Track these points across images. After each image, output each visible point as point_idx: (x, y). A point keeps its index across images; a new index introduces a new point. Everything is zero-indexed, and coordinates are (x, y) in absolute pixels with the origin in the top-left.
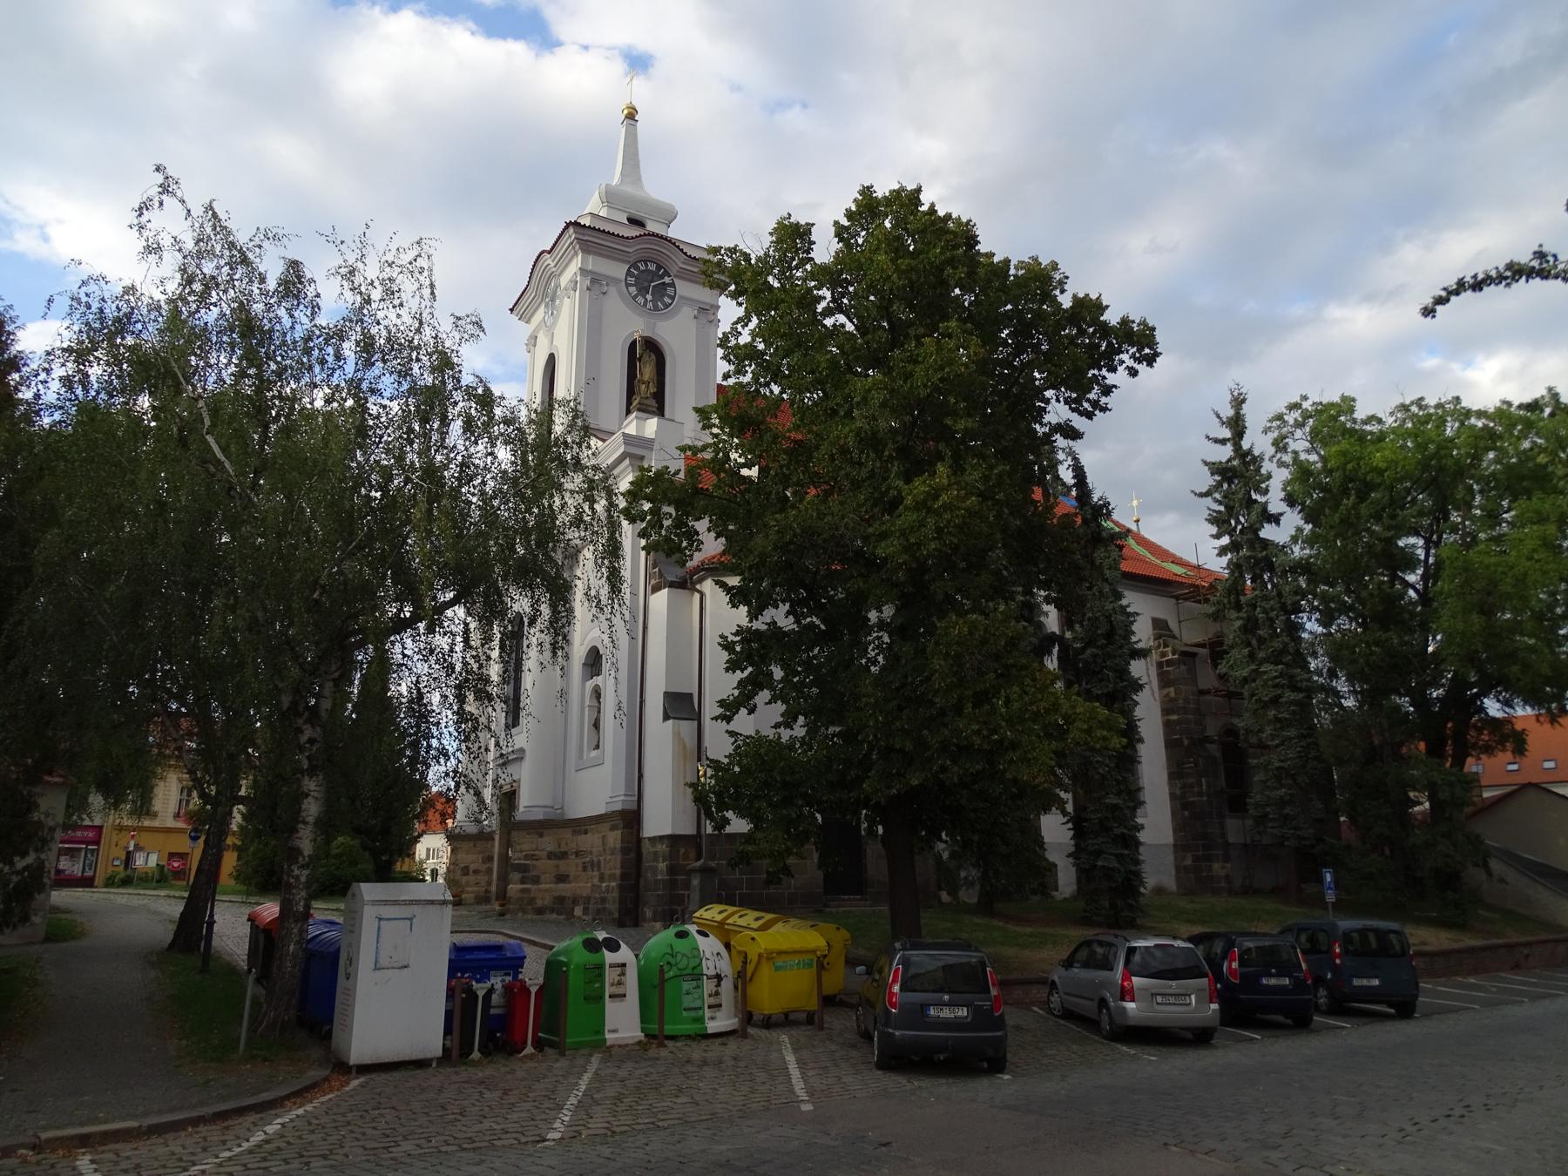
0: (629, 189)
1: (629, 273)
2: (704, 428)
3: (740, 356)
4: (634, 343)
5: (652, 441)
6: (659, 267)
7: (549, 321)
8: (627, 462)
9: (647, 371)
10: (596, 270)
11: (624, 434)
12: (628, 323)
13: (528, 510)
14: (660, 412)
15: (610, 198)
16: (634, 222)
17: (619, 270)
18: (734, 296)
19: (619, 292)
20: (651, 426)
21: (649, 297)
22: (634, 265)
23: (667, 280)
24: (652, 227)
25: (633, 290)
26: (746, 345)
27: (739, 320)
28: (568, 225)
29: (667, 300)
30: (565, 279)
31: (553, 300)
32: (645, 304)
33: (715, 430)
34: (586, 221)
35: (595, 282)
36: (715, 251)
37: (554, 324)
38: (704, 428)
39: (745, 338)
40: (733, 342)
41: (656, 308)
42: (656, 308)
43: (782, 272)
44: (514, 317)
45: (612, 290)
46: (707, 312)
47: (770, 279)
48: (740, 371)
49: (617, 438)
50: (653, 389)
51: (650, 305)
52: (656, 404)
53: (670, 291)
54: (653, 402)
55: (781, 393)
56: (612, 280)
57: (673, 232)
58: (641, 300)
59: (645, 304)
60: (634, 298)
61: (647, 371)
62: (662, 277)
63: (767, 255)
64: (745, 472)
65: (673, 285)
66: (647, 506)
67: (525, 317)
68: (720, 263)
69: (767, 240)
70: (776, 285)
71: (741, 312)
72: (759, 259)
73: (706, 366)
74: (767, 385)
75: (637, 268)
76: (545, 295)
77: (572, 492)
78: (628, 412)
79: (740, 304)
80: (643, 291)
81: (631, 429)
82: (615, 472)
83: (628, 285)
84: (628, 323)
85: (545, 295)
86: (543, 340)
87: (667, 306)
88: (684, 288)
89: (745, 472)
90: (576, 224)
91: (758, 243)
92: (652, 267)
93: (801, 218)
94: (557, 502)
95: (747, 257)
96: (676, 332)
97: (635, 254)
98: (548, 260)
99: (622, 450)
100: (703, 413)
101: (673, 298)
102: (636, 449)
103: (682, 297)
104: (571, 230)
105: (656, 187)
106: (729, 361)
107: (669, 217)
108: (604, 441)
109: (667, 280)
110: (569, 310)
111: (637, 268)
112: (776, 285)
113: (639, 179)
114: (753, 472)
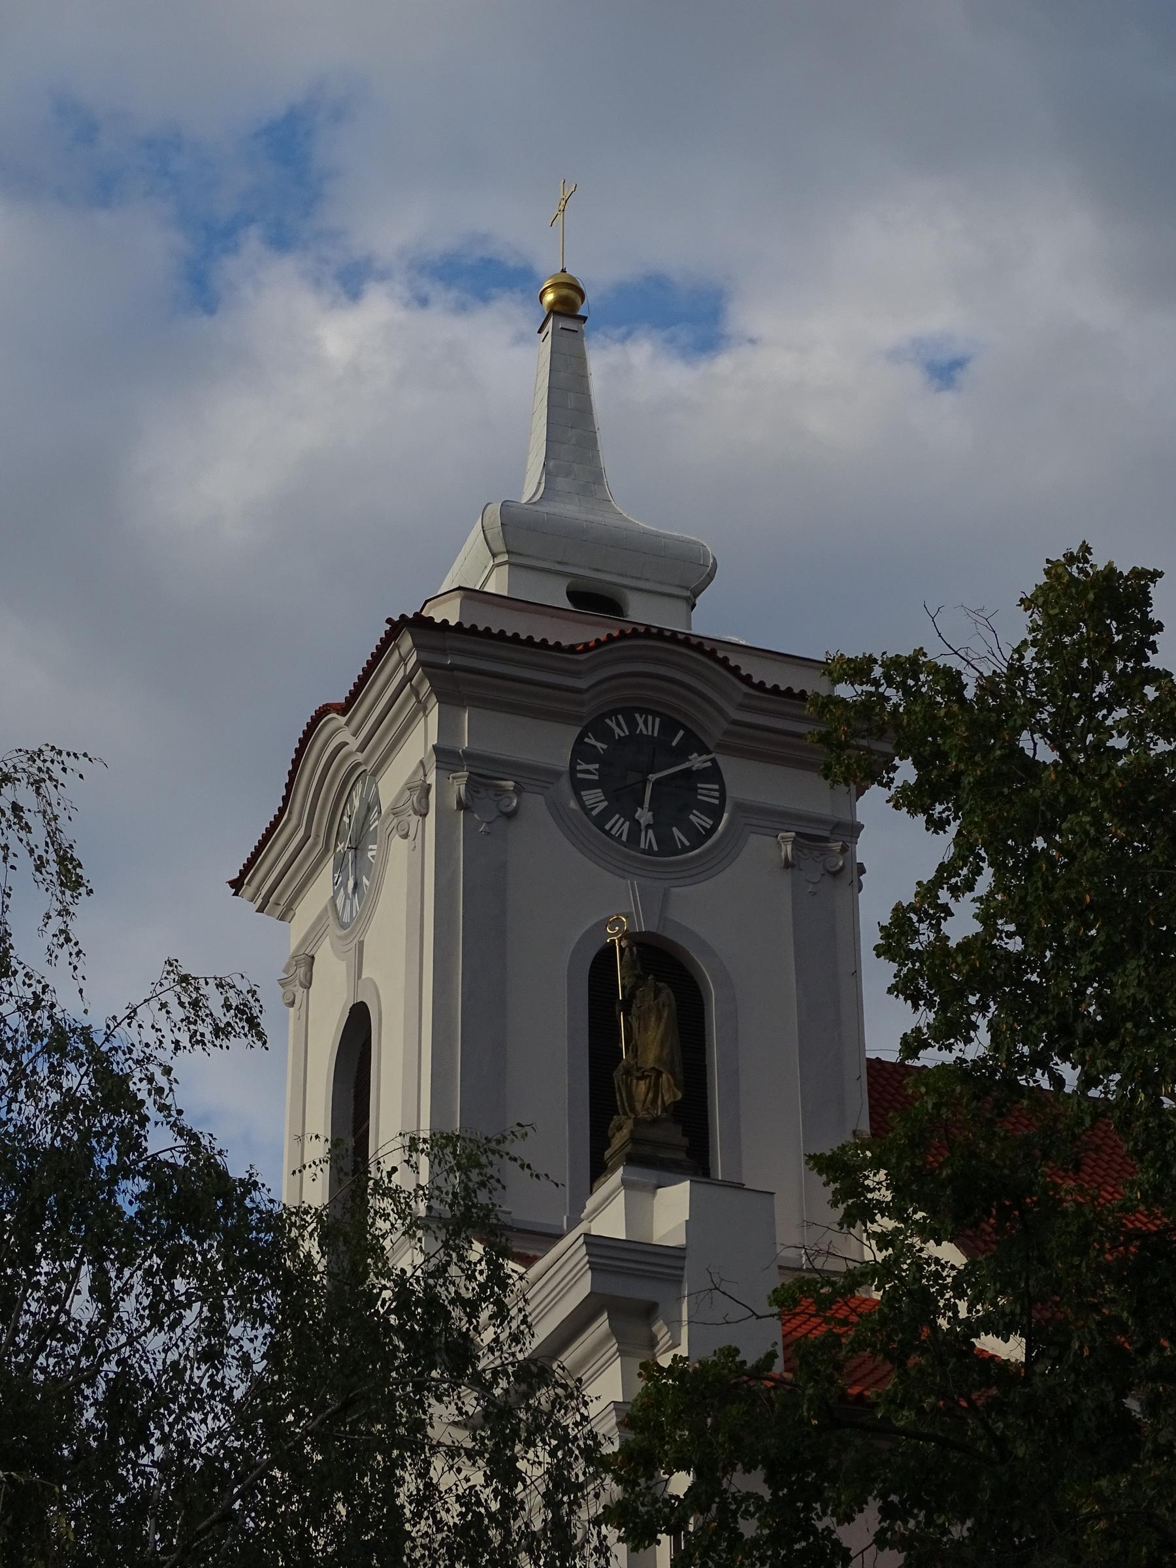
0: (570, 510)
1: (580, 751)
2: (848, 1220)
3: (940, 979)
4: (604, 959)
5: (676, 1255)
6: (670, 726)
7: (349, 908)
8: (602, 1325)
9: (648, 1041)
10: (489, 748)
11: (593, 1242)
12: (589, 899)
13: (317, 1510)
14: (694, 1160)
15: (518, 536)
16: (592, 600)
17: (550, 745)
18: (912, 800)
19: (557, 810)
20: (671, 1211)
21: (644, 816)
22: (596, 727)
23: (697, 761)
24: (642, 611)
25: (595, 798)
26: (966, 946)
27: (945, 871)
28: (396, 628)
29: (698, 819)
30: (392, 784)
31: (357, 847)
32: (634, 837)
33: (886, 1224)
34: (448, 612)
35: (481, 787)
36: (858, 670)
37: (364, 917)
38: (848, 1220)
39: (962, 924)
40: (926, 935)
41: (667, 846)
42: (667, 846)
43: (1064, 719)
44: (245, 906)
45: (535, 803)
46: (826, 852)
47: (1025, 741)
48: (952, 1028)
49: (569, 1253)
50: (670, 1094)
51: (648, 838)
52: (679, 1142)
53: (707, 792)
54: (675, 1134)
55: (1088, 1081)
56: (532, 777)
57: (708, 620)
58: (619, 826)
59: (634, 837)
60: (600, 821)
61: (648, 1041)
62: (682, 753)
63: (1016, 670)
64: (988, 1343)
65: (714, 774)
66: (680, 1483)
67: (277, 903)
68: (870, 706)
69: (1017, 627)
70: (1046, 754)
71: (942, 846)
72: (988, 686)
73: (830, 1005)
74: (1041, 1061)
75: (604, 734)
76: (333, 832)
77: (453, 1452)
78: (599, 1170)
79: (937, 825)
80: (623, 799)
81: (610, 1218)
82: (569, 1358)
83: (578, 786)
84: (589, 899)
85: (333, 832)
86: (331, 969)
87: (699, 837)
88: (746, 781)
89: (988, 1343)
90: (419, 624)
91: (984, 632)
92: (649, 727)
93: (1116, 553)
94: (410, 1484)
95: (951, 680)
96: (728, 913)
97: (594, 697)
98: (341, 732)
99: (584, 1288)
100: (839, 1170)
101: (715, 813)
102: (631, 1282)
103: (742, 808)
104: (407, 642)
105: (641, 497)
106: (915, 998)
107: (691, 575)
108: (528, 1261)
109: (697, 761)
110: (406, 872)
111: (604, 734)
112: (1046, 754)
113: (598, 477)
114: (1011, 1349)
